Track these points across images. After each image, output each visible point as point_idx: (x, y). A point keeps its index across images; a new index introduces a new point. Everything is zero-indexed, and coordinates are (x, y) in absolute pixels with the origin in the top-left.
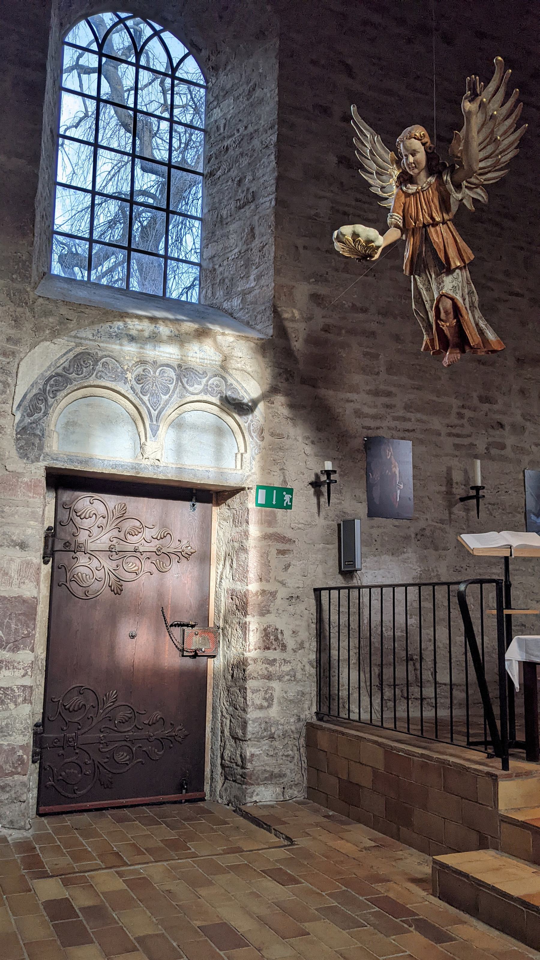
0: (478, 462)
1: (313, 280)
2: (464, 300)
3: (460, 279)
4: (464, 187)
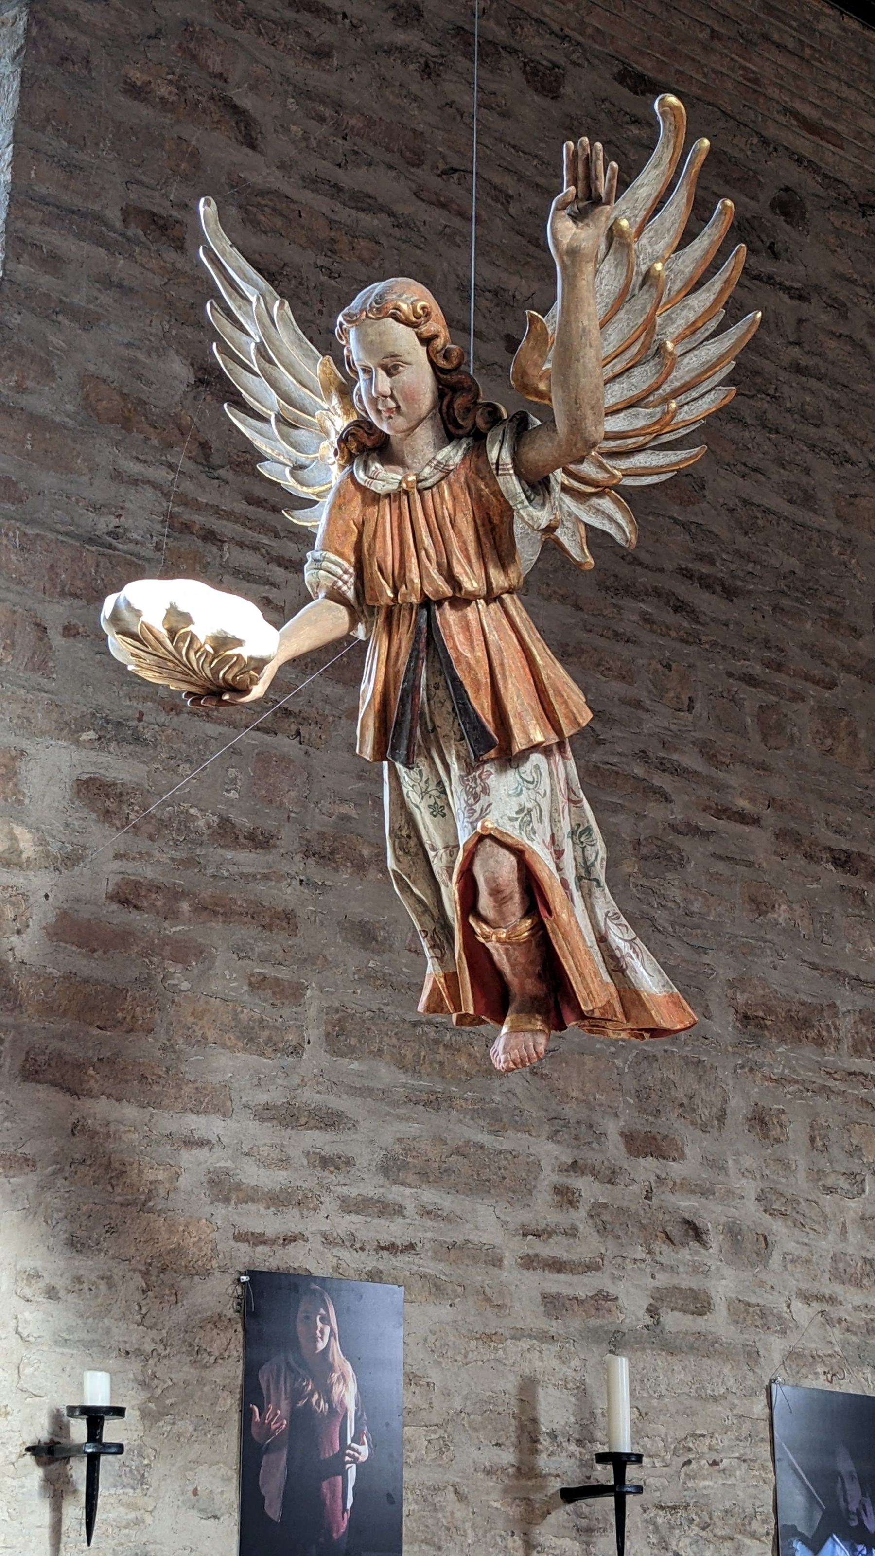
0: (622, 1366)
1: (92, 735)
2: (559, 854)
3: (545, 784)
4: (557, 488)
